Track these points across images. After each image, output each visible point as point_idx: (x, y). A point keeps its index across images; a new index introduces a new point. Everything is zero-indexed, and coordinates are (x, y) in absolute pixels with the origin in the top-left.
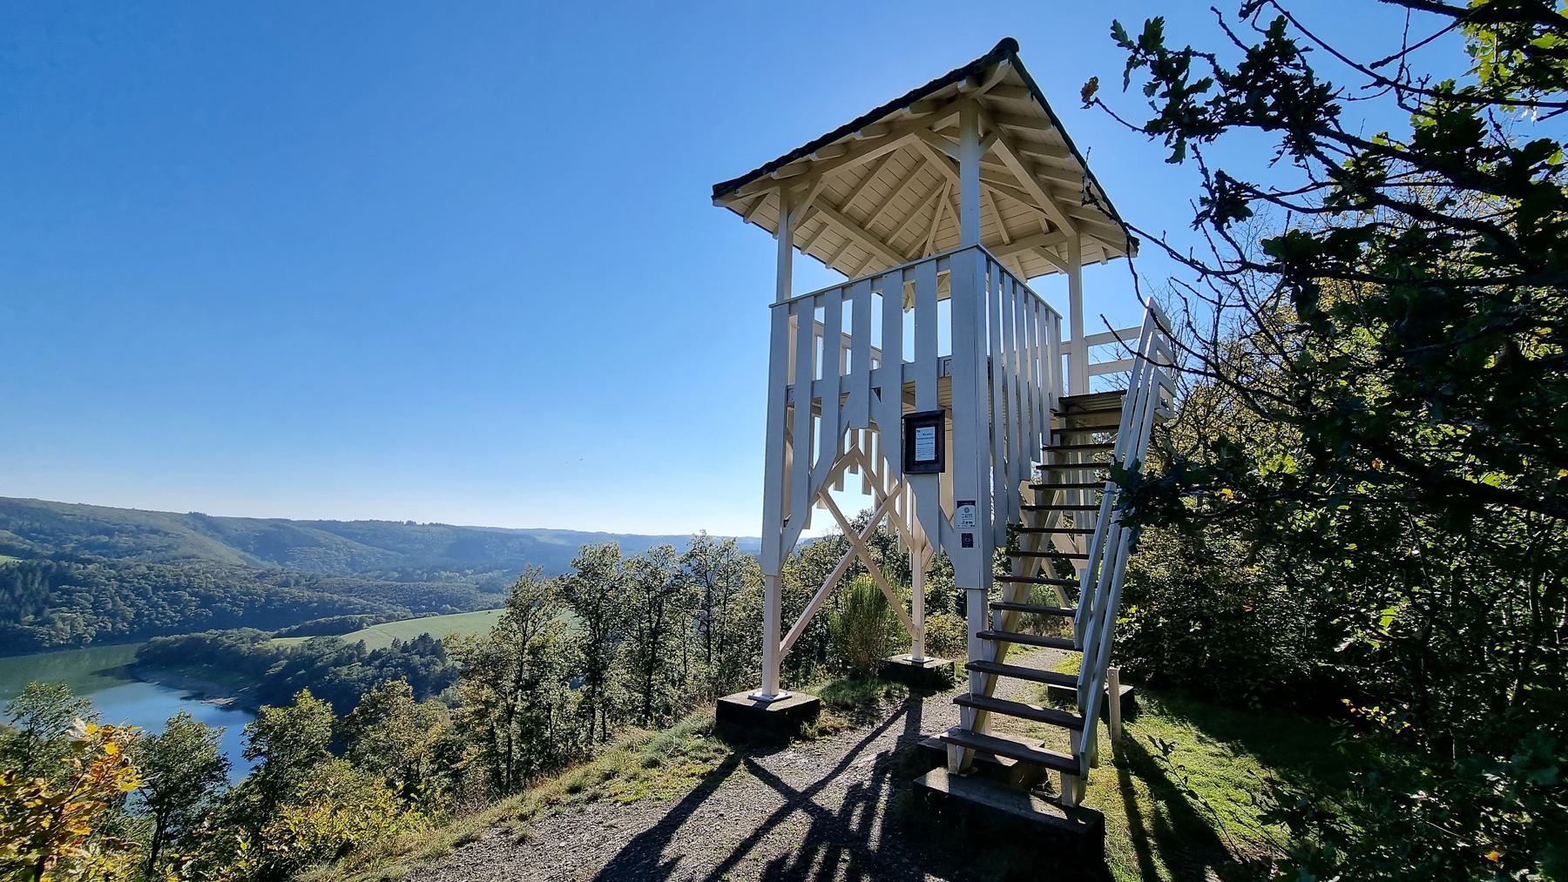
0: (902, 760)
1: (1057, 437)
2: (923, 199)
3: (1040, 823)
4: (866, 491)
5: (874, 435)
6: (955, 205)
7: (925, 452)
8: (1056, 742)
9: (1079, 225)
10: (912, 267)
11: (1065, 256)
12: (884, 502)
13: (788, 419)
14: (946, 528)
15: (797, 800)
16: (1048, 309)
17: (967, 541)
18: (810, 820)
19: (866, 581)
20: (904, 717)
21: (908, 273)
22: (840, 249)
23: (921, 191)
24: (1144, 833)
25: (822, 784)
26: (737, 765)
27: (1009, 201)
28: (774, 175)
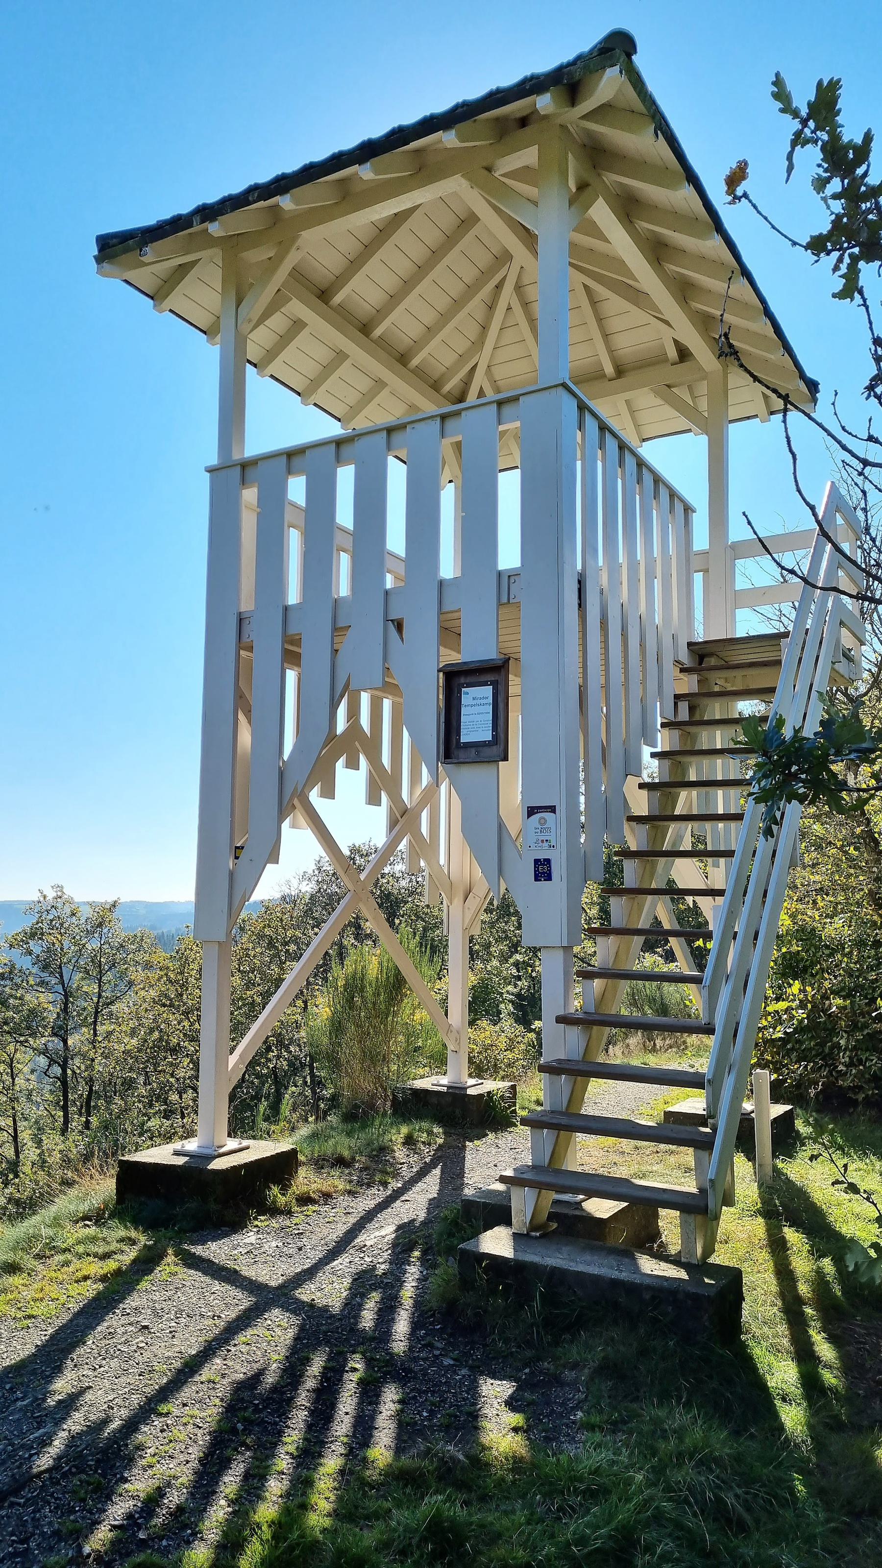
0: (437, 1227)
1: (684, 706)
2: (471, 290)
3: (649, 1287)
4: (373, 799)
5: (387, 704)
6: (526, 305)
7: (476, 724)
8: (671, 1171)
9: (728, 352)
10: (457, 413)
11: (703, 405)
12: (401, 819)
13: (242, 672)
14: (509, 853)
15: (265, 1298)
16: (673, 495)
17: (543, 870)
18: (296, 1320)
19: (371, 963)
20: (437, 1172)
21: (450, 424)
22: (328, 370)
23: (469, 274)
24: (799, 1301)
25: (309, 1274)
26: (161, 1256)
27: (613, 303)
28: (214, 228)
